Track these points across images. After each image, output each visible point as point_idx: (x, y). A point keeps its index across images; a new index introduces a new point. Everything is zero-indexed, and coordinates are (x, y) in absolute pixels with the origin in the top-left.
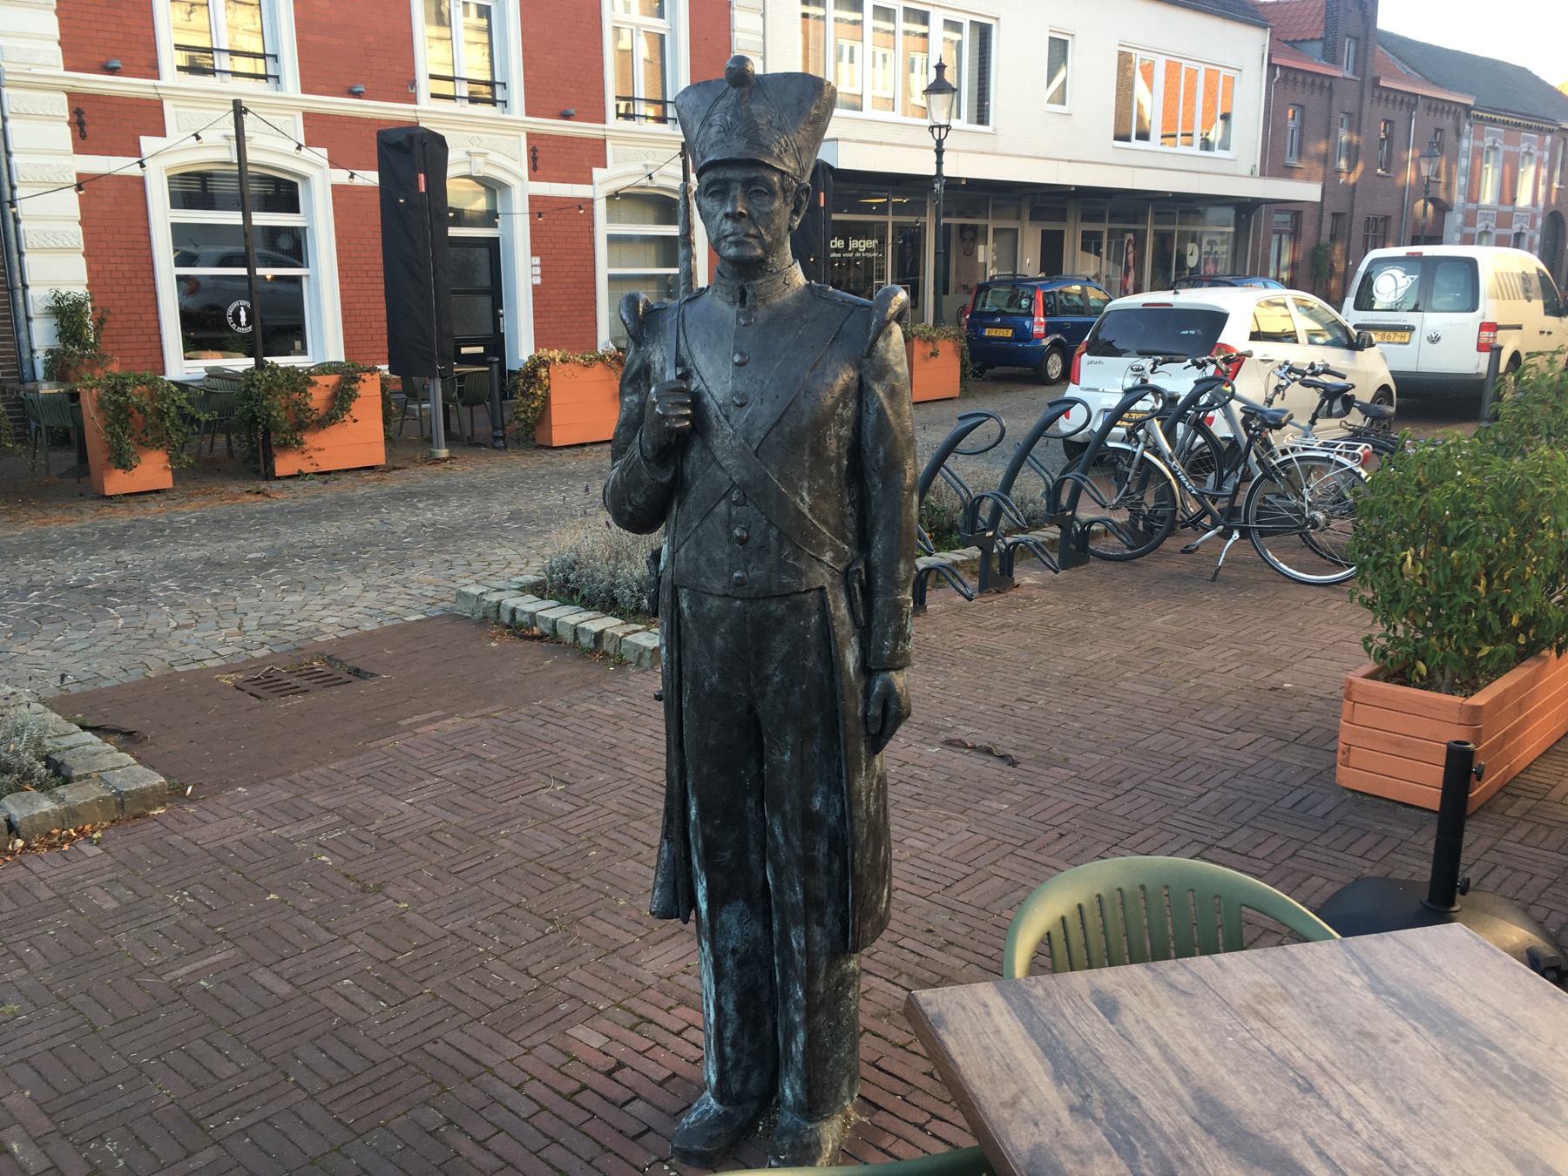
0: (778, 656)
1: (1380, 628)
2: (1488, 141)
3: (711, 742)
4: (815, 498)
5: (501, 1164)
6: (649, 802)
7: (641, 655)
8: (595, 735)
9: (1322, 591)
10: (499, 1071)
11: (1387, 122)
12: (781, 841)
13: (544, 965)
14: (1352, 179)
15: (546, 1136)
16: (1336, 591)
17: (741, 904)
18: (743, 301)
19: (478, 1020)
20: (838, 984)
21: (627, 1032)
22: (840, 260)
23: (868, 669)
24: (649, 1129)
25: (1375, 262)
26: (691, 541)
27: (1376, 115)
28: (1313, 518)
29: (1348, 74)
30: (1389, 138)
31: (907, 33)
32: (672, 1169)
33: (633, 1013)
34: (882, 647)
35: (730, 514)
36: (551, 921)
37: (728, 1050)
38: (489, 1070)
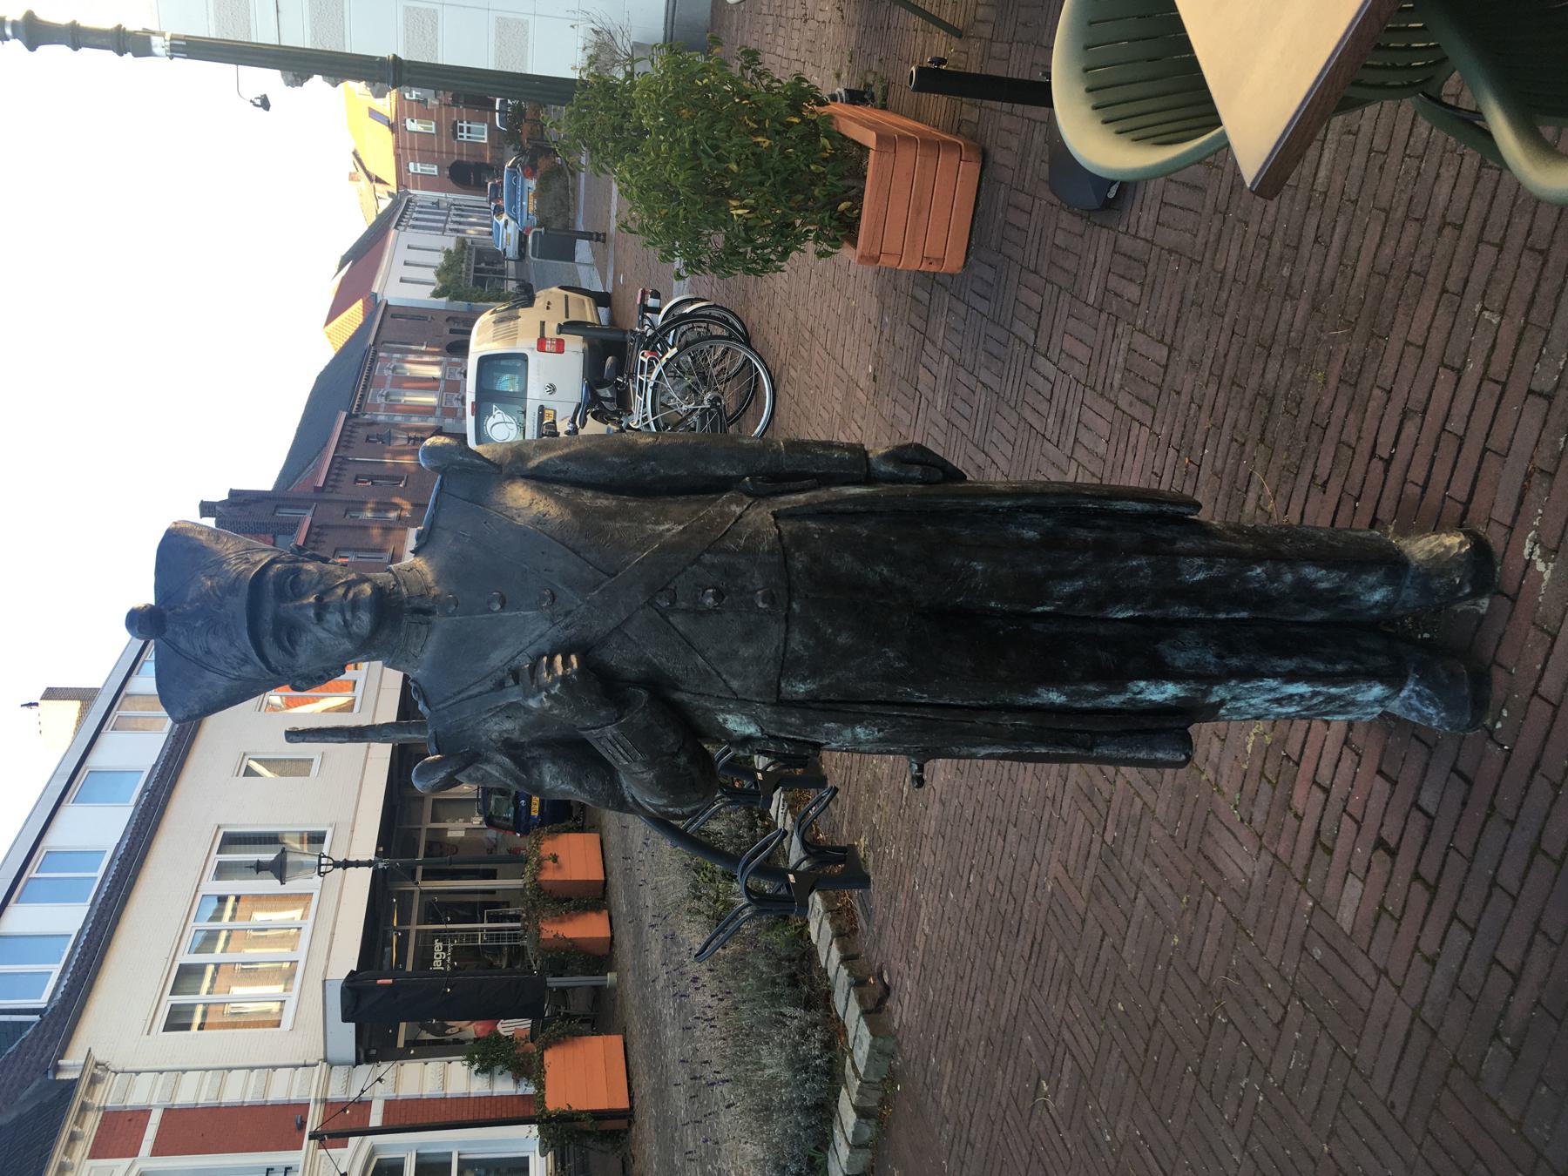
1: (810, 246)
4: (666, 519)
5: (1538, 937)
6: (1050, 964)
7: (880, 1052)
8: (978, 1070)
9: (780, 392)
10: (1415, 1000)
11: (356, 481)
13: (1268, 1004)
14: (407, 505)
15: (1489, 895)
18: (428, 612)
19: (1352, 1059)
21: (1336, 855)
23: (869, 478)
24: (1454, 769)
25: (478, 442)
26: (721, 669)
27: (347, 490)
30: (372, 478)
31: (232, 918)
32: (1499, 717)
33: (1310, 859)
34: (841, 460)
35: (686, 611)
36: (1212, 1019)
37: (1339, 667)
38: (1416, 1015)
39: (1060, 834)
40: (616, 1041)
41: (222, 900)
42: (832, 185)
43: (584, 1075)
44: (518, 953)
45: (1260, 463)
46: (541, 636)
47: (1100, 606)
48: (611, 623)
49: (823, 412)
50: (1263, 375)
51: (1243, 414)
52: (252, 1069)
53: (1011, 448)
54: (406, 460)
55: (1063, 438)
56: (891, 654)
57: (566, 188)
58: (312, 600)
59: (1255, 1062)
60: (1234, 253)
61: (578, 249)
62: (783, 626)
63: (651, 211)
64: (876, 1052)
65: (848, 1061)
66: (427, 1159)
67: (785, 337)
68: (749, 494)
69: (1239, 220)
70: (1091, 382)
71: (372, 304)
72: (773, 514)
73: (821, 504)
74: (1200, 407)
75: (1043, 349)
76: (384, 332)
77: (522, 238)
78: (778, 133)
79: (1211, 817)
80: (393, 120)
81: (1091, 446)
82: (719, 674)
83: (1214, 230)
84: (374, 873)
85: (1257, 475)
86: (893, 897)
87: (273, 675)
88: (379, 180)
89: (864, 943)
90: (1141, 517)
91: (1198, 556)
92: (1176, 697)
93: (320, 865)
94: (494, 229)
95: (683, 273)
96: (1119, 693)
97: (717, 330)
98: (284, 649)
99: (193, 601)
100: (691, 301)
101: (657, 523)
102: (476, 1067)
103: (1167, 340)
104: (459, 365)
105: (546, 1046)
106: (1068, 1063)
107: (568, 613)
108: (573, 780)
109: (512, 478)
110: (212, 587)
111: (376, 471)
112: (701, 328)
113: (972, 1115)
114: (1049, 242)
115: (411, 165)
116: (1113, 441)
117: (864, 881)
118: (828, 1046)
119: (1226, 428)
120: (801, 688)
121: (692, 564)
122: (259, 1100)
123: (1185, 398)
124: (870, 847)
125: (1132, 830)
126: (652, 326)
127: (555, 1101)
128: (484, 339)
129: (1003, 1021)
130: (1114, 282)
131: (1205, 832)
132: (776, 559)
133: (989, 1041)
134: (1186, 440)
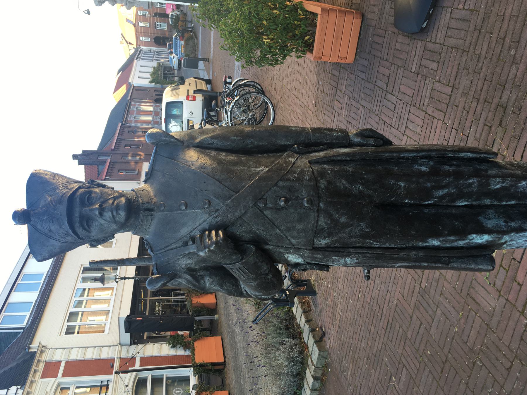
0: (348, 186)
1: (294, 54)
2: (133, 119)
3: (398, 229)
6: (395, 334)
7: (322, 357)
8: (364, 369)
9: (277, 112)
11: (125, 146)
12: (446, 191)
13: (504, 360)
16: (277, 108)
17: (481, 218)
20: (513, 166)
22: (162, 311)
23: (350, 145)
26: (287, 234)
27: (122, 149)
28: (251, 116)
29: (110, 157)
30: (130, 146)
31: (88, 296)
34: (337, 137)
35: (271, 208)
36: (474, 364)
39: (400, 282)
40: (219, 338)
41: (84, 290)
42: (303, 29)
43: (208, 350)
44: (184, 306)
45: (500, 134)
46: (204, 221)
47: (454, 201)
48: (237, 215)
49: (294, 119)
50: (501, 97)
51: (490, 114)
52: (95, 347)
53: (411, 130)
54: (142, 139)
55: (400, 126)
56: (364, 226)
57: (195, 44)
58: (97, 206)
59: (496, 383)
60: (485, 47)
61: (199, 65)
62: (316, 215)
63: (233, 42)
64: (321, 357)
65: (309, 359)
66: (154, 377)
67: (278, 92)
68: (297, 153)
69: (488, 32)
70: (413, 103)
71: (129, 85)
72: (309, 162)
73: (330, 157)
74: (468, 112)
75: (390, 91)
76: (133, 95)
77: (180, 61)
78: (282, 9)
79: (474, 281)
80: (134, 23)
81: (414, 129)
82: (287, 237)
83: (475, 37)
84: (135, 281)
85: (498, 140)
86: (326, 299)
87: (81, 241)
88: (130, 43)
89: (314, 315)
90: (471, 160)
91: (498, 177)
92: (487, 241)
93: (116, 279)
94: (169, 59)
95: (245, 66)
96: (463, 240)
97: (252, 90)
98: (85, 229)
99: (43, 207)
100: (242, 80)
101: (256, 167)
102: (171, 345)
103: (451, 84)
104: (159, 106)
105: (195, 340)
106: (404, 371)
107: (217, 211)
108: (219, 285)
109: (188, 147)
110: (51, 201)
111: (131, 143)
112: (246, 89)
113: (361, 385)
114: (393, 48)
115: (141, 38)
116: (425, 127)
117: (314, 293)
118: (301, 352)
119: (482, 120)
120: (323, 242)
121: (274, 186)
122: (98, 358)
123: (460, 107)
124: (316, 280)
125: (434, 284)
126: (229, 89)
127: (199, 360)
128: (168, 96)
129: (374, 352)
130: (424, 62)
131: (471, 286)
132: (312, 183)
133: (368, 358)
134: (461, 126)
